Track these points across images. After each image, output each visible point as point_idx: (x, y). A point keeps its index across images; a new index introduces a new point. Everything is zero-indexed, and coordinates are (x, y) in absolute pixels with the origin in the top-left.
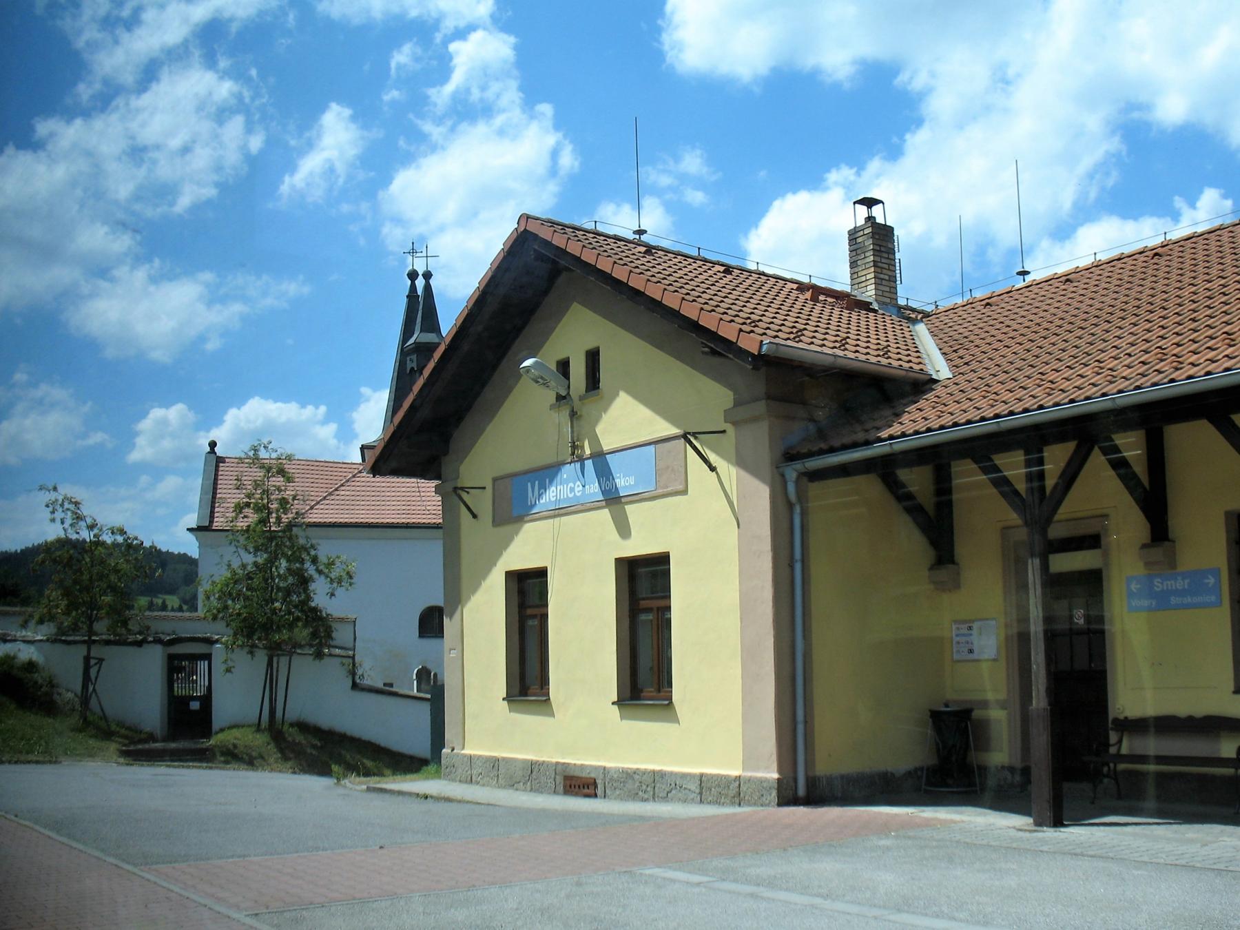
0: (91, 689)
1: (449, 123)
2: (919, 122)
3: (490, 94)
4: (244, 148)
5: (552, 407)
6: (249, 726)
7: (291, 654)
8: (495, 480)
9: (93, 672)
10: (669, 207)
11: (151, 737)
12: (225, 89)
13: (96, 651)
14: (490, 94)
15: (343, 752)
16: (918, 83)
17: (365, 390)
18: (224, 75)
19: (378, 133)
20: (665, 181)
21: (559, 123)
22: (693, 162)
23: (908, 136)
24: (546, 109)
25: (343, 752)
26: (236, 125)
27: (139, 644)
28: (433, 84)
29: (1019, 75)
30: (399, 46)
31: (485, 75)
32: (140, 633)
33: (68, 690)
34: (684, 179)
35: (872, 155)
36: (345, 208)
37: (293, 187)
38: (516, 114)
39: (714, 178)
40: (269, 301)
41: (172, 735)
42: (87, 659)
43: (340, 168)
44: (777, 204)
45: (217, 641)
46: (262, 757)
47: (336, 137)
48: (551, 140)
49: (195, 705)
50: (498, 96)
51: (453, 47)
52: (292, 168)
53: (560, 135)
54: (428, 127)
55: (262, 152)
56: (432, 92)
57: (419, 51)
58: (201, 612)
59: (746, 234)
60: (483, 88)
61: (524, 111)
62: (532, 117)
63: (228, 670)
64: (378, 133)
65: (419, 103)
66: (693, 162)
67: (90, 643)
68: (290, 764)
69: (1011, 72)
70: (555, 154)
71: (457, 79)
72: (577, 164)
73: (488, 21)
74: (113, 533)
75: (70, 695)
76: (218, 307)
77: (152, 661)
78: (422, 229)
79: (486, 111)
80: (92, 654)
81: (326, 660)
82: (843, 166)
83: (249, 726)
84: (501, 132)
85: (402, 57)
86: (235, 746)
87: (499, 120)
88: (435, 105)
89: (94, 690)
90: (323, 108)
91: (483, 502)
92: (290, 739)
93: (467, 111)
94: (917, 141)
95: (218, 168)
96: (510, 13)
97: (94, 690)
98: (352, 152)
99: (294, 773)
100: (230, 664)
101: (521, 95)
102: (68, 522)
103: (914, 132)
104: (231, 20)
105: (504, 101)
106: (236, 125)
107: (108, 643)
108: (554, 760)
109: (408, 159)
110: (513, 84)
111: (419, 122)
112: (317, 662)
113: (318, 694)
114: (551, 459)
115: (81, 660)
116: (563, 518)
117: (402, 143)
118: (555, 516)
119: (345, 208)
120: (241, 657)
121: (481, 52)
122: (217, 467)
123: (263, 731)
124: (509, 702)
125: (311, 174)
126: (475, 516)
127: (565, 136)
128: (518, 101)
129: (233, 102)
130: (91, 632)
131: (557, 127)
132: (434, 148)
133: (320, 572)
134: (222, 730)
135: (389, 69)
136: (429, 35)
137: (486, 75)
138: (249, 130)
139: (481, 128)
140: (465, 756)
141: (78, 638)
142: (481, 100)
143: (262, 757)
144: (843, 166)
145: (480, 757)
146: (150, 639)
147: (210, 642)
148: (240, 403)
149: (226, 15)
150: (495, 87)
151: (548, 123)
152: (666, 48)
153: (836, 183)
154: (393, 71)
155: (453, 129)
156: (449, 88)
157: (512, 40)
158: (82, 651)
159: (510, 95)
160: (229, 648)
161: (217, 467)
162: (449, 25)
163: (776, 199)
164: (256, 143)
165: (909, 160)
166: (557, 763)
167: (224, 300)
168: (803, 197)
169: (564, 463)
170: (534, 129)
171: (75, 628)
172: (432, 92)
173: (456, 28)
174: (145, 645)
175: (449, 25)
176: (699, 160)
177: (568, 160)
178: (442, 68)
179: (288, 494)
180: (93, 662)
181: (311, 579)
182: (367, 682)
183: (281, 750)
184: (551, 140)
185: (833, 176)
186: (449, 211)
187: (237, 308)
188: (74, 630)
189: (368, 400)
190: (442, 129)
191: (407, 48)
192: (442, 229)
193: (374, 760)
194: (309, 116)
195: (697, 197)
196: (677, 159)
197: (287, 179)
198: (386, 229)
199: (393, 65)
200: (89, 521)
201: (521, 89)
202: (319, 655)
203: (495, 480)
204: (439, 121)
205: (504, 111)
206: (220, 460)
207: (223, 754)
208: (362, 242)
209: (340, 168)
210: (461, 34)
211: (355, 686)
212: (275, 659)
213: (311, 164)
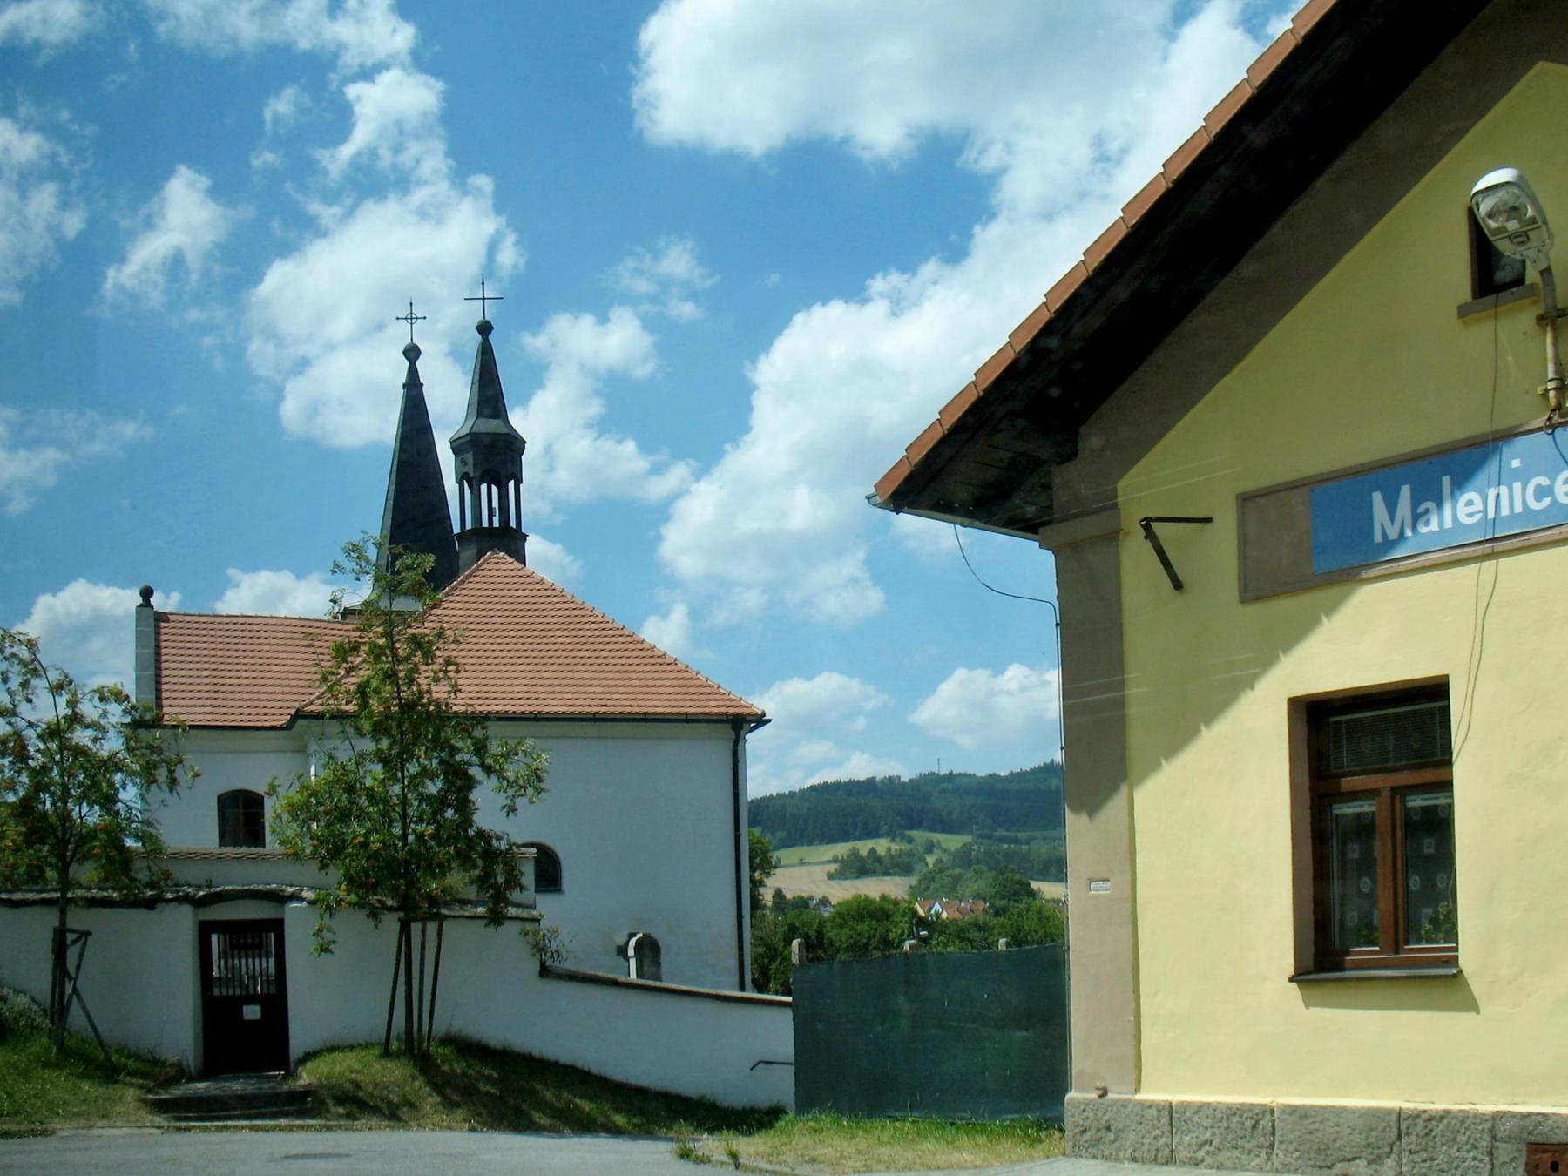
0: (69, 989)
1: (349, 201)
2: (986, 213)
3: (406, 158)
4: (53, 229)
5: (1463, 311)
6: (367, 1046)
7: (440, 919)
8: (1245, 499)
9: (72, 954)
10: (648, 324)
11: (181, 1074)
12: (28, 147)
13: (78, 919)
14: (406, 158)
15: (539, 1087)
16: (991, 161)
17: (232, 572)
18: (25, 127)
19: (248, 212)
20: (642, 286)
21: (501, 204)
22: (678, 261)
23: (977, 229)
24: (483, 182)
25: (539, 1087)
26: (44, 199)
27: (150, 904)
28: (324, 145)
29: (1124, 151)
30: (278, 90)
31: (399, 132)
32: (151, 885)
33: (18, 992)
34: (666, 283)
35: (925, 259)
36: (194, 315)
37: (119, 287)
38: (443, 187)
39: (708, 283)
40: (97, 447)
41: (210, 1069)
42: (60, 935)
43: (193, 260)
44: (799, 319)
45: (295, 897)
46: (411, 1105)
47: (186, 215)
48: (490, 225)
49: (252, 1012)
50: (418, 161)
51: (353, 91)
52: (120, 258)
53: (502, 220)
54: (314, 207)
55: (81, 236)
56: (323, 156)
57: (307, 100)
58: (272, 844)
59: (754, 359)
60: (397, 149)
61: (453, 185)
62: (465, 193)
63: (324, 949)
64: (248, 212)
65: (303, 169)
66: (678, 261)
67: (63, 904)
68: (460, 1114)
69: (1113, 147)
70: (493, 247)
71: (360, 137)
72: (522, 261)
73: (408, 59)
74: (102, 699)
75: (23, 1000)
76: (22, 453)
77: (174, 931)
78: (302, 350)
79: (401, 182)
80: (70, 924)
81: (508, 925)
82: (892, 270)
83: (367, 1046)
84: (423, 214)
85: (282, 105)
86: (357, 1085)
87: (419, 196)
88: (326, 173)
89: (75, 990)
90: (168, 173)
91: (1216, 555)
92: (446, 1068)
93: (373, 182)
94: (988, 237)
95: (20, 260)
96: (437, 48)
97: (75, 990)
98: (208, 238)
99: (473, 1130)
100: (327, 936)
101: (450, 162)
102: (15, 683)
103: (985, 225)
104: (38, 45)
105: (425, 170)
106: (44, 199)
107: (93, 903)
108: (1487, 1108)
109: (287, 249)
110: (439, 146)
111: (299, 197)
112: (491, 929)
113: (487, 990)
114: (1480, 426)
115: (49, 935)
116: (1506, 563)
117: (276, 225)
118: (1493, 555)
119: (194, 315)
120: (350, 926)
121: (393, 99)
122: (157, 627)
123: (397, 1055)
124: (1298, 982)
125: (145, 268)
126: (1178, 585)
127: (508, 225)
128: (444, 170)
129: (46, 163)
130: (66, 884)
131: (499, 208)
132: (323, 234)
133: (488, 770)
134: (309, 1056)
135: (263, 122)
136: (321, 76)
137: (401, 132)
138: (65, 204)
139: (392, 206)
140: (1141, 1103)
141: (30, 896)
142: (394, 167)
143: (411, 1105)
144: (892, 270)
145: (1200, 1108)
146: (169, 896)
147: (279, 898)
148: (55, 589)
149: (29, 38)
150: (414, 149)
151: (488, 203)
152: (634, 105)
153: (881, 295)
154: (268, 127)
155: (350, 213)
156: (347, 151)
157: (440, 85)
158: (48, 920)
159: (432, 160)
160: (325, 905)
161: (157, 627)
162: (350, 60)
163: (795, 312)
164: (73, 224)
165: (977, 264)
166: (1498, 1116)
167: (32, 444)
168: (836, 310)
169: (1510, 434)
170: (467, 205)
171: (35, 876)
172: (323, 156)
173: (362, 66)
174: (160, 906)
175: (350, 60)
176: (686, 258)
177: (508, 256)
178: (341, 119)
179: (427, 629)
180: (70, 937)
181: (470, 783)
182: (568, 965)
183: (438, 1088)
184: (490, 225)
185: (878, 285)
186: (343, 325)
187: (51, 455)
188: (35, 880)
189: (237, 586)
190: (336, 210)
191: (290, 93)
192: (331, 347)
193: (591, 1099)
194: (151, 184)
195: (687, 310)
196: (657, 255)
197: (111, 273)
198: (253, 347)
199: (268, 115)
200: (54, 676)
201: (450, 154)
202: (496, 918)
203: (1245, 499)
204: (331, 197)
205: (426, 183)
206: (161, 617)
207: (341, 1100)
208: (218, 363)
209: (193, 260)
210: (368, 74)
211: (545, 972)
212: (416, 927)
213: (149, 251)
